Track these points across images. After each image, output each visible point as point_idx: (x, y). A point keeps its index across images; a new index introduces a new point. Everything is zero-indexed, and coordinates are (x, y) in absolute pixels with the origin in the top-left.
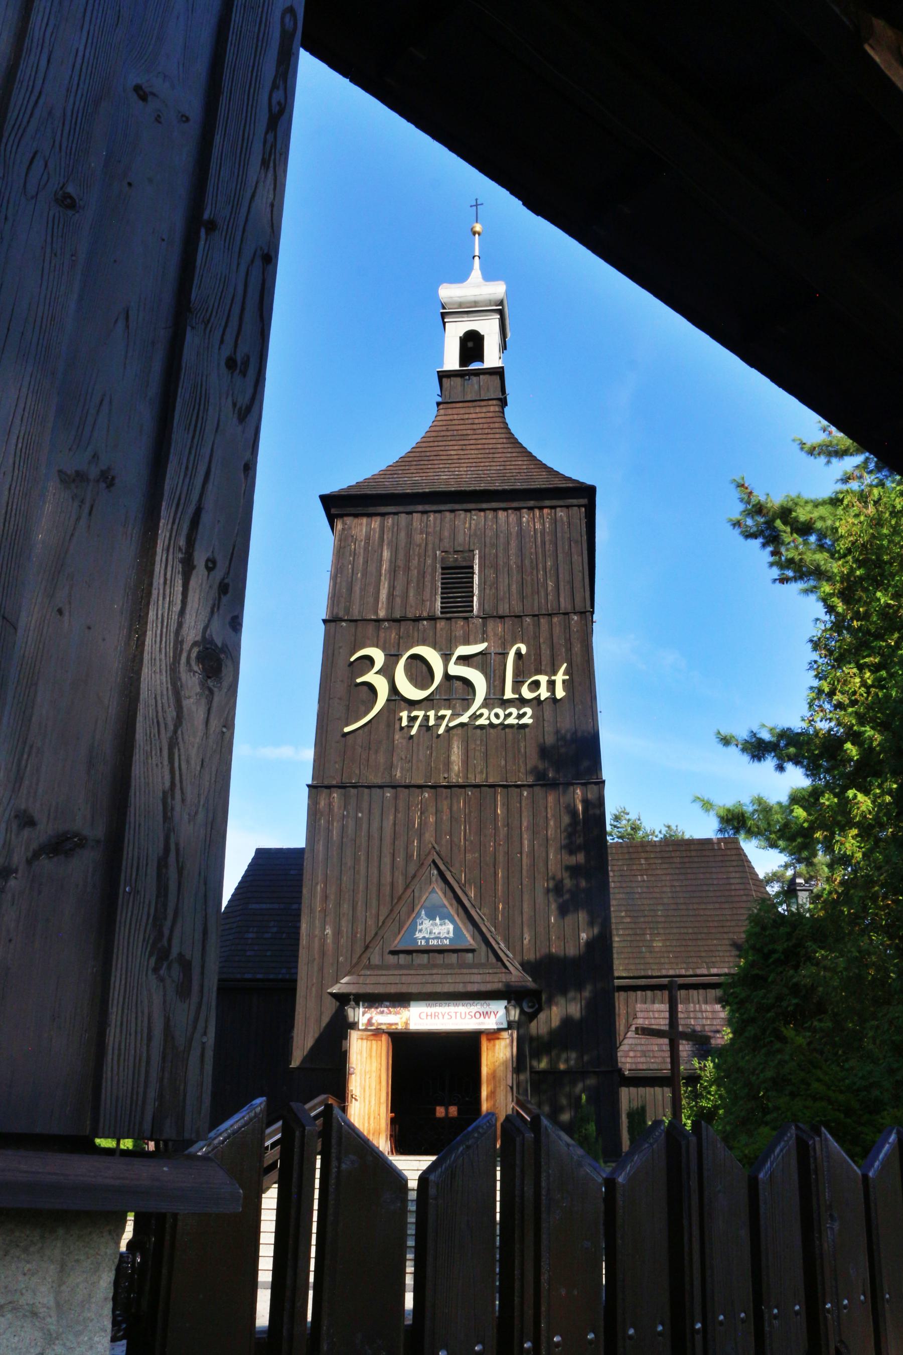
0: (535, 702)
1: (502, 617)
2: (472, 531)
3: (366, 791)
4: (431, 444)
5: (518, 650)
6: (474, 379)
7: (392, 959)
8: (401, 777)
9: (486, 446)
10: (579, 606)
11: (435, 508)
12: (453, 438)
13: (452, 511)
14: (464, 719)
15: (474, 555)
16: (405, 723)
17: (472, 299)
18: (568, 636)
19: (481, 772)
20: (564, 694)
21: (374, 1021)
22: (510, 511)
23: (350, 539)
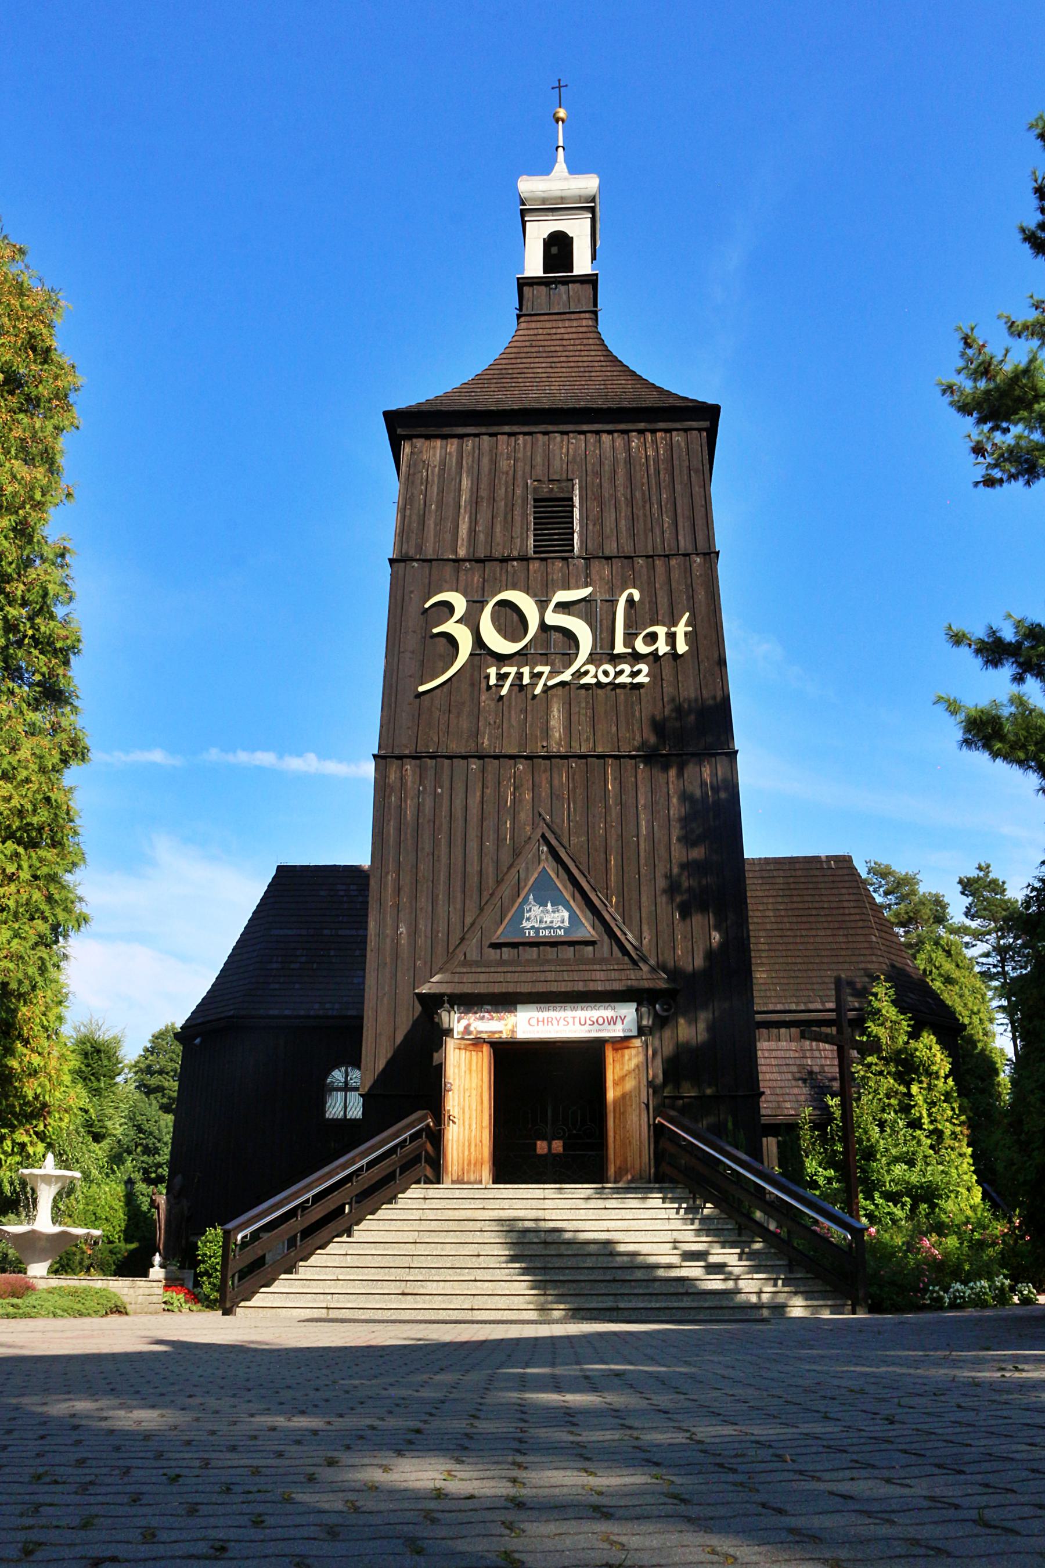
0: (651, 658)
1: (608, 558)
2: (570, 458)
3: (447, 762)
4: (513, 361)
5: (631, 595)
6: (562, 288)
7: (493, 954)
8: (490, 745)
9: (580, 364)
10: (702, 547)
11: (526, 429)
12: (538, 355)
13: (545, 433)
14: (566, 676)
15: (573, 485)
16: (493, 681)
17: (559, 194)
18: (689, 582)
19: (588, 740)
20: (687, 648)
21: (472, 1029)
22: (616, 435)
23: (421, 464)
